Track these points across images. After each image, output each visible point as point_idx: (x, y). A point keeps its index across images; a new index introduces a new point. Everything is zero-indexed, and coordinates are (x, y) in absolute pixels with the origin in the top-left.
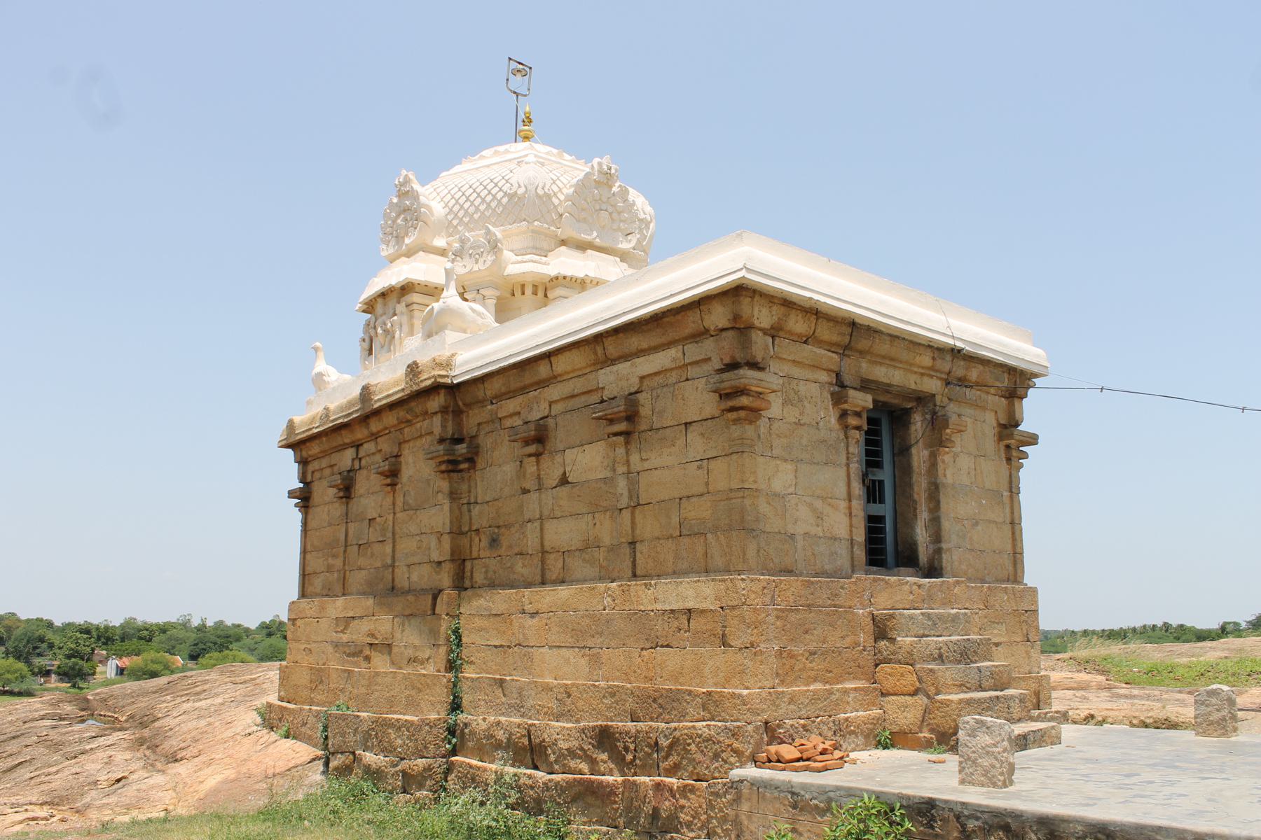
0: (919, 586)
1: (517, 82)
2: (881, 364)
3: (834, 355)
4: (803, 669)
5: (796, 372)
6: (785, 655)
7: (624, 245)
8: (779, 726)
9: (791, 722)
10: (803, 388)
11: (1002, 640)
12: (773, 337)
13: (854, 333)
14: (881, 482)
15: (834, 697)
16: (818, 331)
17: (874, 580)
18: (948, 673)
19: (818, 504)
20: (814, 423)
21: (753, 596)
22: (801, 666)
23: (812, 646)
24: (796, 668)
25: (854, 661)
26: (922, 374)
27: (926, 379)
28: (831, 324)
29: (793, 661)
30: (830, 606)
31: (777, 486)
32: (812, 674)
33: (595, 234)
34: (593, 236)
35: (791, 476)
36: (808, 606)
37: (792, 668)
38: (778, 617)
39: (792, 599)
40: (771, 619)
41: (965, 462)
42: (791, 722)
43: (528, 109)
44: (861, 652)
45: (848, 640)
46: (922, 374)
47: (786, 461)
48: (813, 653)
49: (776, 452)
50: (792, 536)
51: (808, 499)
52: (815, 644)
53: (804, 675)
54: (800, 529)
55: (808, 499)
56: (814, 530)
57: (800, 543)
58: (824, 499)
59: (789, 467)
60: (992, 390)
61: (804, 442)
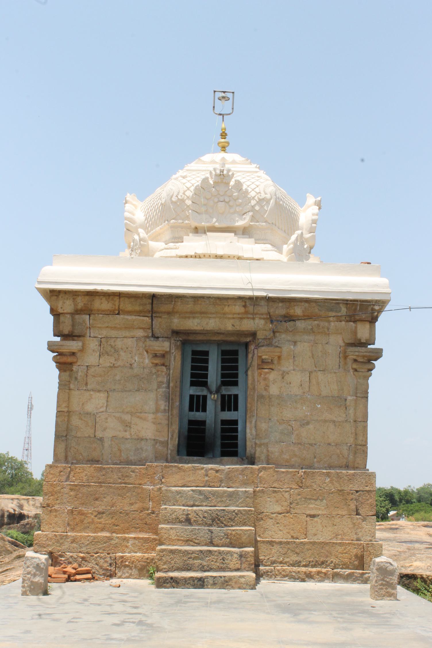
0: (217, 471)
1: (224, 107)
2: (189, 318)
3: (145, 318)
4: (93, 522)
5: (113, 333)
6: (75, 513)
7: (240, 223)
8: (61, 556)
9: (71, 554)
10: (119, 344)
11: (320, 512)
12: (89, 315)
13: (153, 304)
14: (236, 397)
15: (113, 542)
16: (121, 306)
17: (166, 467)
18: (172, 532)
19: (127, 418)
20: (128, 365)
21: (51, 476)
22: (90, 520)
23: (100, 509)
24: (85, 521)
25: (141, 520)
26: (241, 318)
27: (245, 321)
28: (133, 300)
29: (83, 517)
30: (121, 483)
31: (90, 407)
32: (100, 526)
33: (214, 220)
34: (215, 222)
35: (104, 401)
36: (100, 483)
37: (82, 521)
38: (71, 490)
39: (85, 478)
40: (66, 490)
41: (297, 378)
42: (71, 554)
43: (223, 126)
44: (149, 514)
45: (136, 506)
46: (241, 318)
47: (99, 391)
48: (100, 513)
49: (89, 387)
50: (101, 440)
51: (117, 415)
52: (104, 507)
53: (93, 526)
54: (108, 434)
55: (117, 415)
56: (121, 434)
57: (107, 444)
58: (132, 414)
59: (103, 395)
60: (331, 319)
61: (118, 378)
